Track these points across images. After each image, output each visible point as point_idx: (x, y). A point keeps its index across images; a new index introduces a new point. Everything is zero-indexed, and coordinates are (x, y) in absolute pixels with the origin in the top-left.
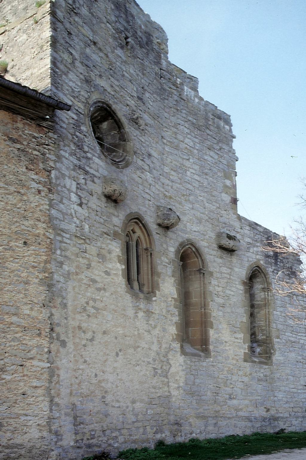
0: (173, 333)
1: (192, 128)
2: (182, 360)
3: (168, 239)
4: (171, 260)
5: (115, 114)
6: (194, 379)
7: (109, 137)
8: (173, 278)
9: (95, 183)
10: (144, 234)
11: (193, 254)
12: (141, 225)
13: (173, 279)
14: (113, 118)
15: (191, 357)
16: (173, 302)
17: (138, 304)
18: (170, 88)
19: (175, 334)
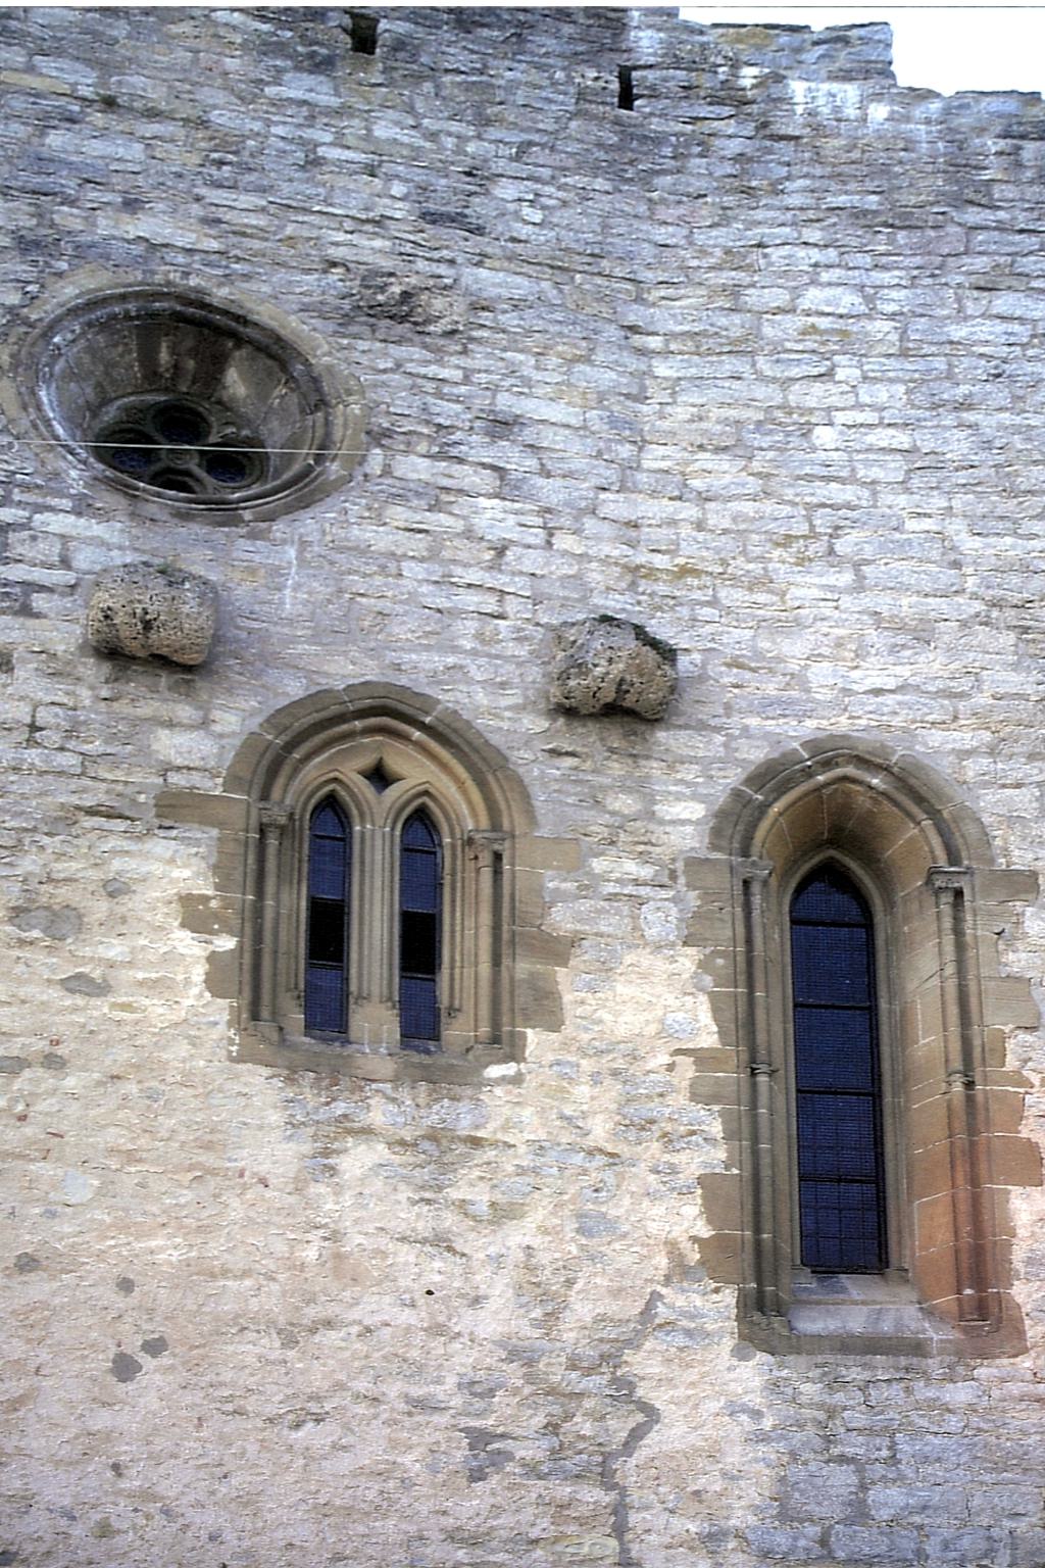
0: (679, 1233)
1: (851, 236)
2: (757, 1382)
3: (655, 768)
4: (680, 866)
5: (242, 320)
6: (863, 1487)
7: (275, 424)
8: (691, 951)
9: (38, 616)
10: (444, 767)
11: (887, 806)
12: (417, 734)
13: (688, 960)
14: (240, 341)
15: (831, 1359)
16: (687, 1069)
17: (340, 1107)
18: (695, 120)
19: (694, 1239)
